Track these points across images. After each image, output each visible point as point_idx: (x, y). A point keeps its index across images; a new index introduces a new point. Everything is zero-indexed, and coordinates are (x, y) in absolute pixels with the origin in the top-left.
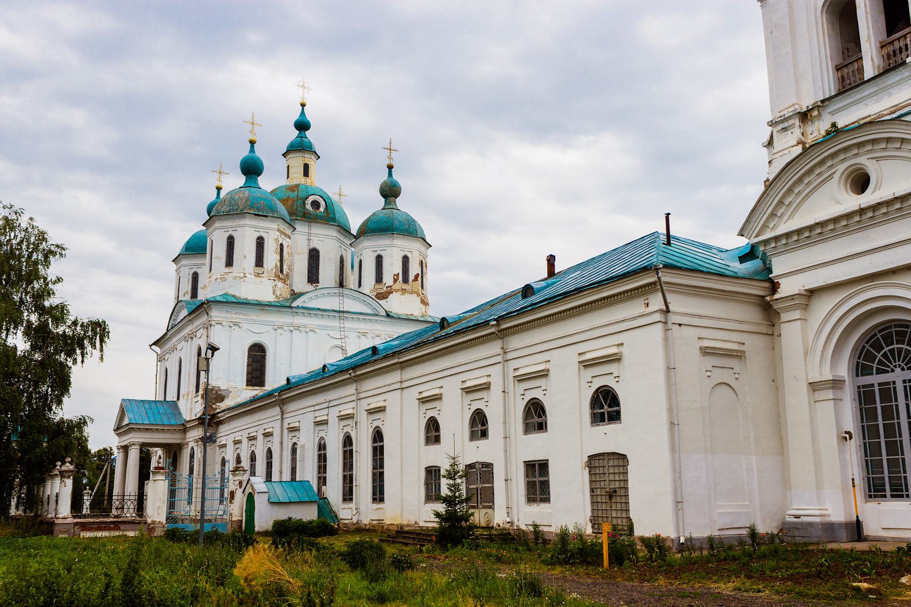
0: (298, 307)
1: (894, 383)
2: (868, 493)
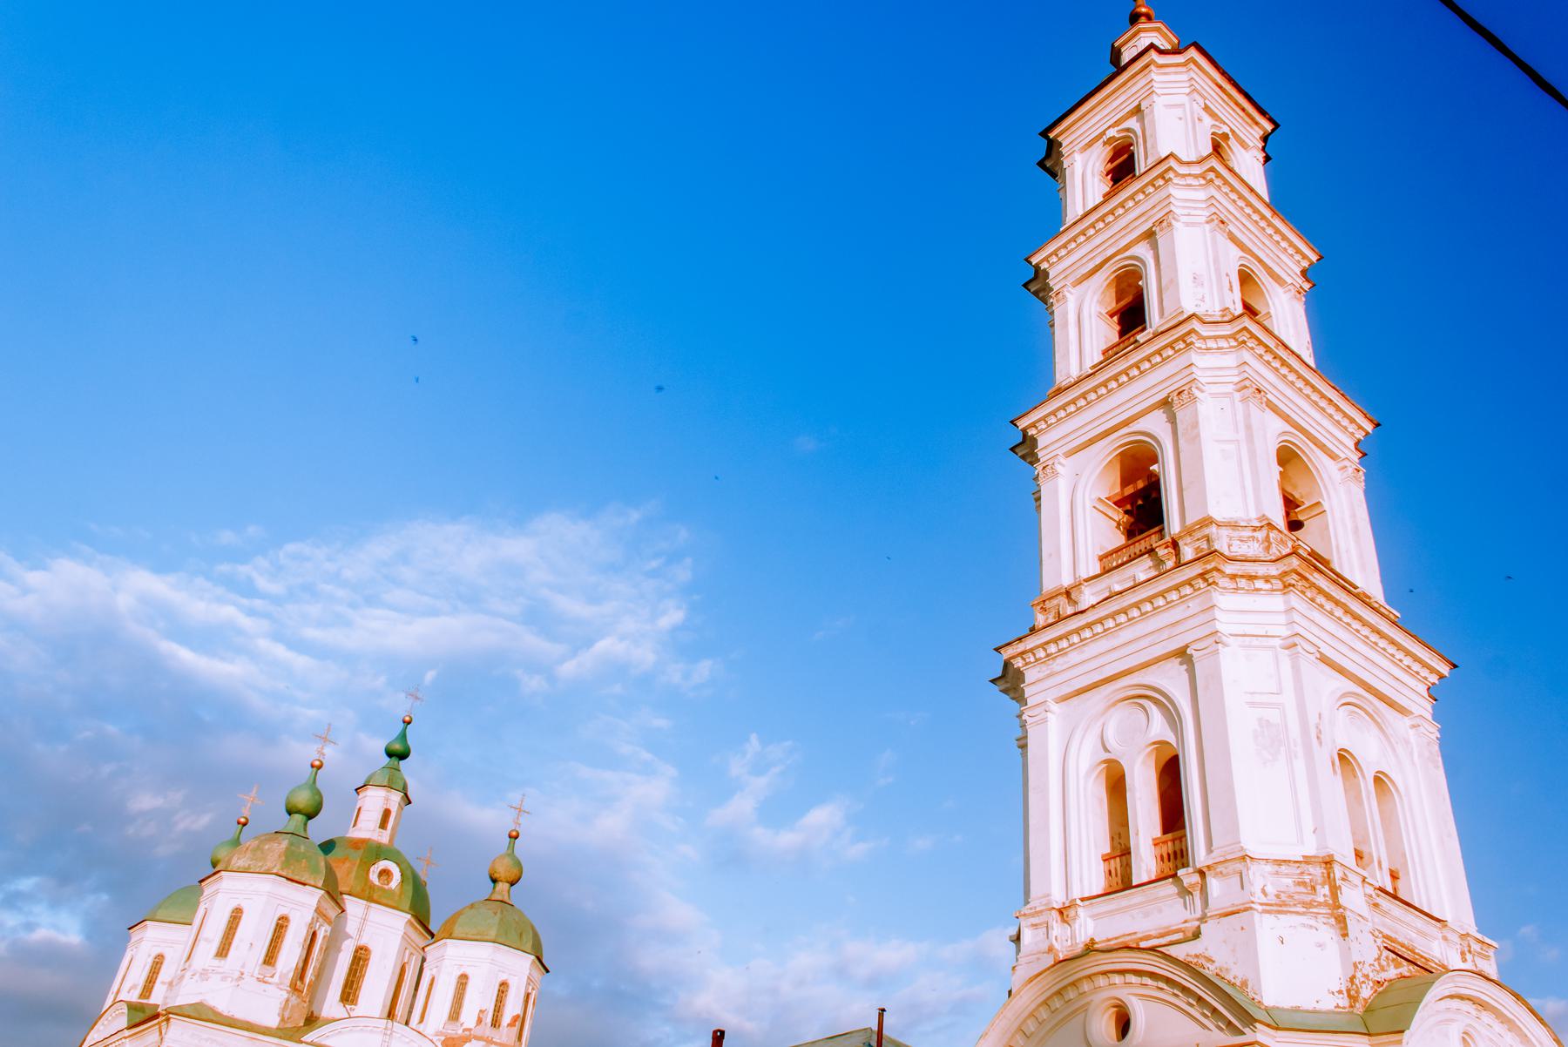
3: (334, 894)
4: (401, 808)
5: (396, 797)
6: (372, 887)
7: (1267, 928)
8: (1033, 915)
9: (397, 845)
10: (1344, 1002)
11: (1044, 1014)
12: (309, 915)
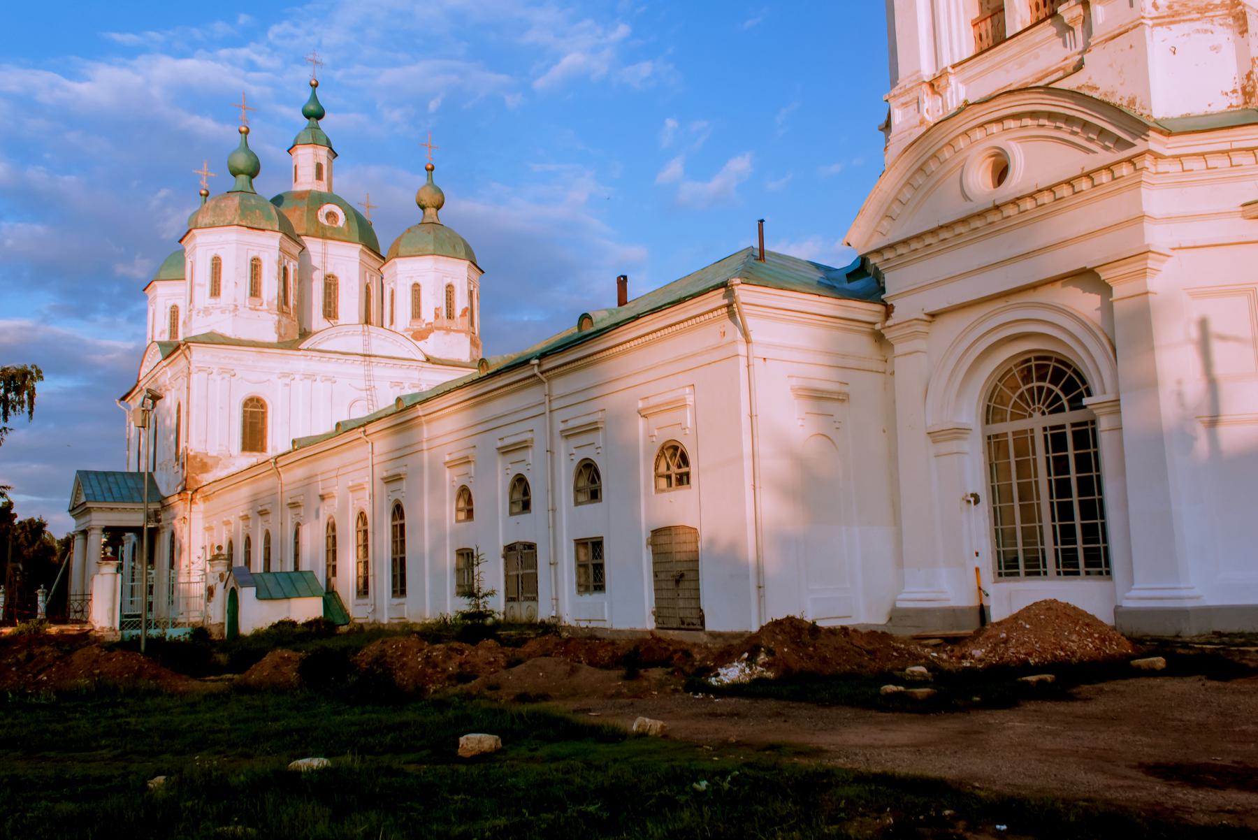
0: (308, 350)
1: (1032, 430)
2: (997, 570)
3: (289, 232)
4: (330, 162)
5: (323, 152)
6: (323, 227)
7: (1158, 41)
8: (901, 95)
9: (336, 191)
10: (1237, 100)
11: (907, 194)
12: (276, 254)
